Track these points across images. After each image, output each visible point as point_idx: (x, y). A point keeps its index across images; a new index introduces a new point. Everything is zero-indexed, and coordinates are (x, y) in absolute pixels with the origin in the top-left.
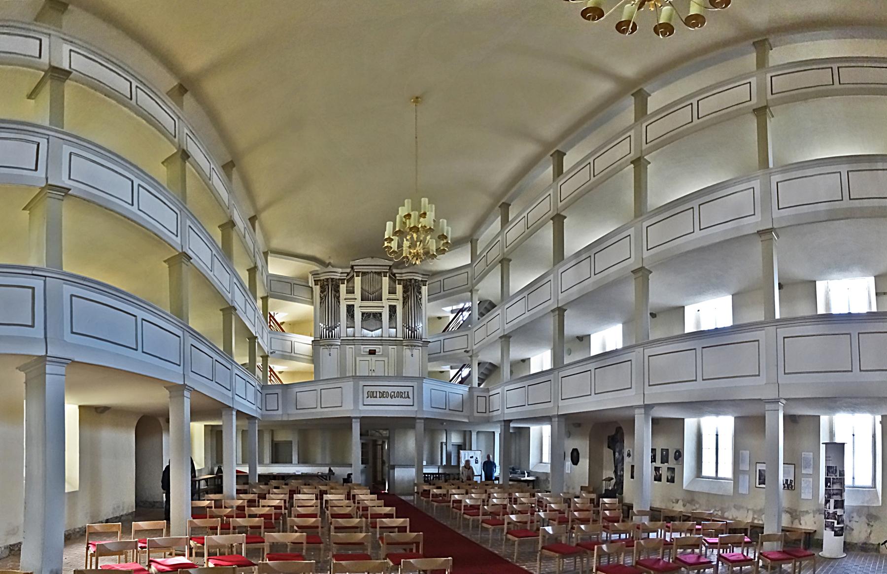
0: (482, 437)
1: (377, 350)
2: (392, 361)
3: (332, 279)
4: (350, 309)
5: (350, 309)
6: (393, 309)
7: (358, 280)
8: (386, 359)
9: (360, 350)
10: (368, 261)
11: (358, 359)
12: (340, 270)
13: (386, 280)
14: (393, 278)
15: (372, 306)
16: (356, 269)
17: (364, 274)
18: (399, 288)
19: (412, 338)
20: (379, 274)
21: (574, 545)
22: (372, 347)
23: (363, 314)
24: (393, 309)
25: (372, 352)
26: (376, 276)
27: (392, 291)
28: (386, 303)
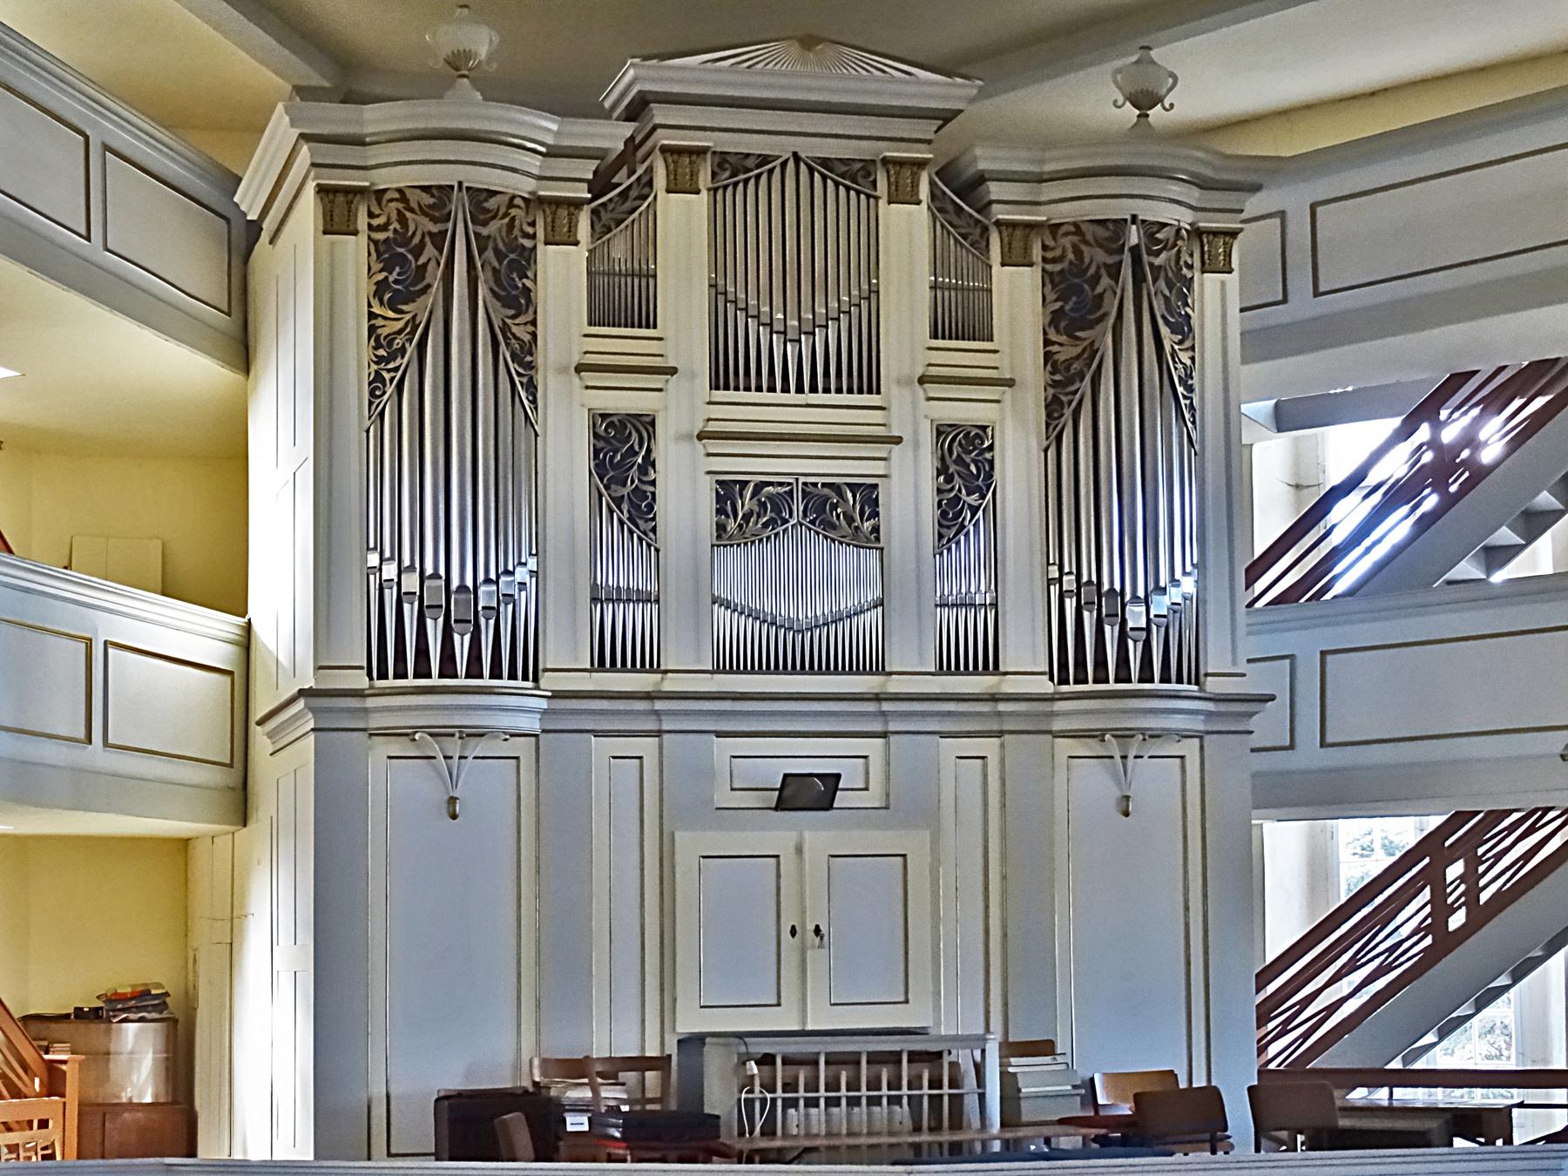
0: (815, 1131)
1: (850, 774)
2: (963, 842)
3: (480, 196)
4: (621, 450)
5: (621, 450)
6: (965, 461)
7: (681, 220)
8: (915, 844)
9: (707, 774)
10: (775, 69)
11: (689, 845)
12: (547, 127)
13: (907, 228)
14: (961, 200)
15: (798, 440)
16: (675, 127)
17: (734, 169)
18: (1017, 295)
19: (1107, 655)
20: (854, 175)
21: (603, 1110)
22: (809, 756)
23: (727, 492)
24: (965, 461)
25: (808, 794)
26: (831, 198)
27: (960, 319)
28: (911, 413)
